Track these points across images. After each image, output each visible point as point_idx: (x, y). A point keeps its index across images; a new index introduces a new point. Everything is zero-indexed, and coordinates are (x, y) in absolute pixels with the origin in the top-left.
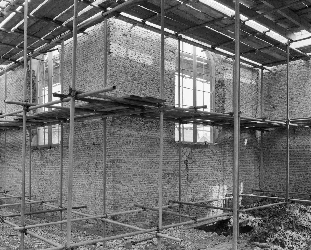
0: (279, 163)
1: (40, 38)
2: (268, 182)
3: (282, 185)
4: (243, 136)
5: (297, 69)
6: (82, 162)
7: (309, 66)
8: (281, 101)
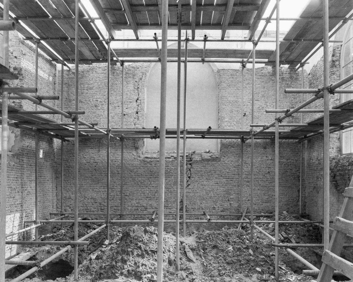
0: (81, 180)
2: (68, 203)
3: (85, 205)
4: (41, 145)
5: (102, 73)
7: (114, 72)
8: (84, 107)
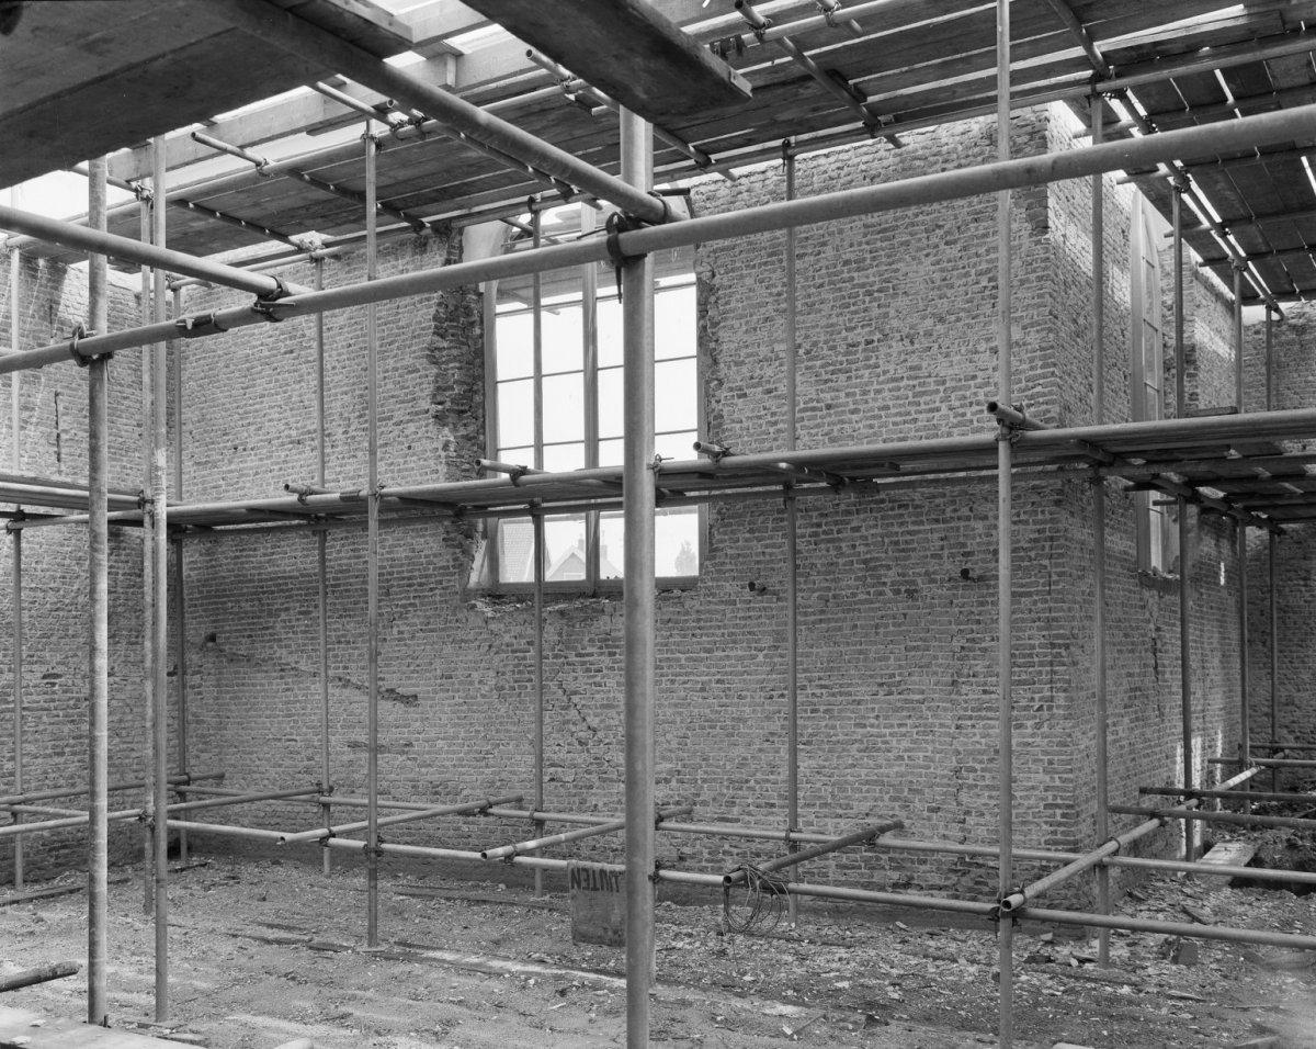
1: (685, 143)
6: (863, 647)
